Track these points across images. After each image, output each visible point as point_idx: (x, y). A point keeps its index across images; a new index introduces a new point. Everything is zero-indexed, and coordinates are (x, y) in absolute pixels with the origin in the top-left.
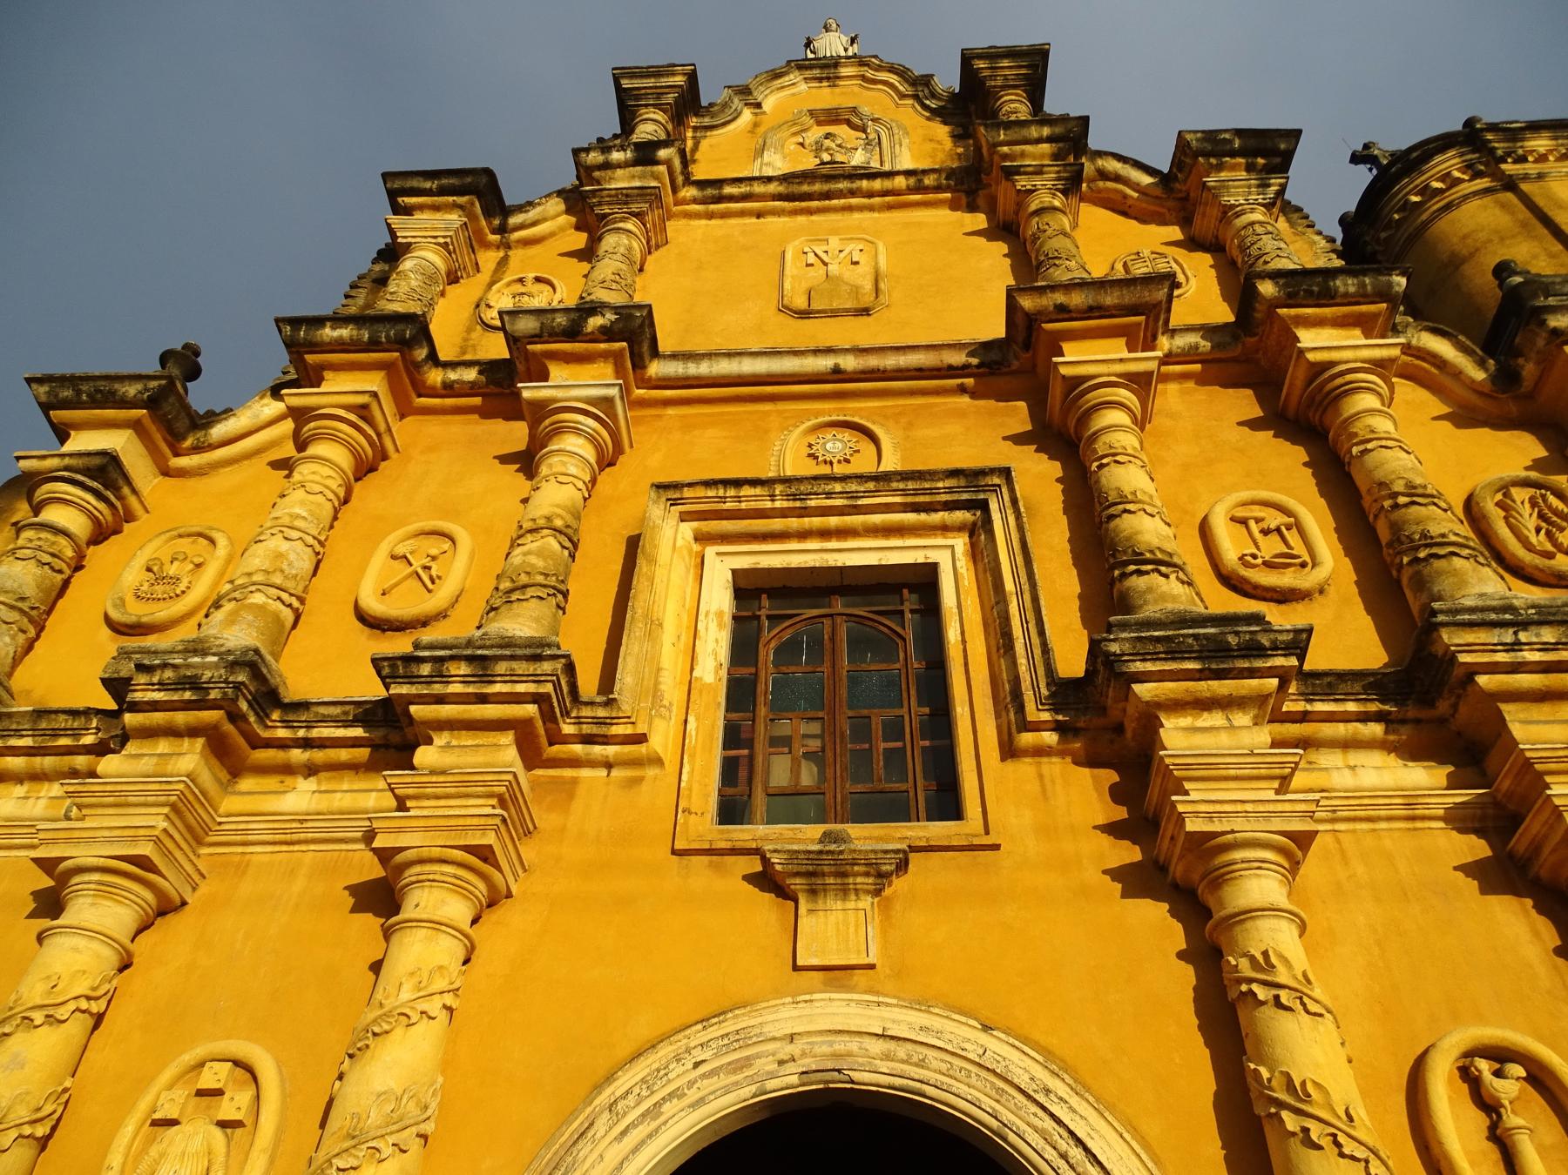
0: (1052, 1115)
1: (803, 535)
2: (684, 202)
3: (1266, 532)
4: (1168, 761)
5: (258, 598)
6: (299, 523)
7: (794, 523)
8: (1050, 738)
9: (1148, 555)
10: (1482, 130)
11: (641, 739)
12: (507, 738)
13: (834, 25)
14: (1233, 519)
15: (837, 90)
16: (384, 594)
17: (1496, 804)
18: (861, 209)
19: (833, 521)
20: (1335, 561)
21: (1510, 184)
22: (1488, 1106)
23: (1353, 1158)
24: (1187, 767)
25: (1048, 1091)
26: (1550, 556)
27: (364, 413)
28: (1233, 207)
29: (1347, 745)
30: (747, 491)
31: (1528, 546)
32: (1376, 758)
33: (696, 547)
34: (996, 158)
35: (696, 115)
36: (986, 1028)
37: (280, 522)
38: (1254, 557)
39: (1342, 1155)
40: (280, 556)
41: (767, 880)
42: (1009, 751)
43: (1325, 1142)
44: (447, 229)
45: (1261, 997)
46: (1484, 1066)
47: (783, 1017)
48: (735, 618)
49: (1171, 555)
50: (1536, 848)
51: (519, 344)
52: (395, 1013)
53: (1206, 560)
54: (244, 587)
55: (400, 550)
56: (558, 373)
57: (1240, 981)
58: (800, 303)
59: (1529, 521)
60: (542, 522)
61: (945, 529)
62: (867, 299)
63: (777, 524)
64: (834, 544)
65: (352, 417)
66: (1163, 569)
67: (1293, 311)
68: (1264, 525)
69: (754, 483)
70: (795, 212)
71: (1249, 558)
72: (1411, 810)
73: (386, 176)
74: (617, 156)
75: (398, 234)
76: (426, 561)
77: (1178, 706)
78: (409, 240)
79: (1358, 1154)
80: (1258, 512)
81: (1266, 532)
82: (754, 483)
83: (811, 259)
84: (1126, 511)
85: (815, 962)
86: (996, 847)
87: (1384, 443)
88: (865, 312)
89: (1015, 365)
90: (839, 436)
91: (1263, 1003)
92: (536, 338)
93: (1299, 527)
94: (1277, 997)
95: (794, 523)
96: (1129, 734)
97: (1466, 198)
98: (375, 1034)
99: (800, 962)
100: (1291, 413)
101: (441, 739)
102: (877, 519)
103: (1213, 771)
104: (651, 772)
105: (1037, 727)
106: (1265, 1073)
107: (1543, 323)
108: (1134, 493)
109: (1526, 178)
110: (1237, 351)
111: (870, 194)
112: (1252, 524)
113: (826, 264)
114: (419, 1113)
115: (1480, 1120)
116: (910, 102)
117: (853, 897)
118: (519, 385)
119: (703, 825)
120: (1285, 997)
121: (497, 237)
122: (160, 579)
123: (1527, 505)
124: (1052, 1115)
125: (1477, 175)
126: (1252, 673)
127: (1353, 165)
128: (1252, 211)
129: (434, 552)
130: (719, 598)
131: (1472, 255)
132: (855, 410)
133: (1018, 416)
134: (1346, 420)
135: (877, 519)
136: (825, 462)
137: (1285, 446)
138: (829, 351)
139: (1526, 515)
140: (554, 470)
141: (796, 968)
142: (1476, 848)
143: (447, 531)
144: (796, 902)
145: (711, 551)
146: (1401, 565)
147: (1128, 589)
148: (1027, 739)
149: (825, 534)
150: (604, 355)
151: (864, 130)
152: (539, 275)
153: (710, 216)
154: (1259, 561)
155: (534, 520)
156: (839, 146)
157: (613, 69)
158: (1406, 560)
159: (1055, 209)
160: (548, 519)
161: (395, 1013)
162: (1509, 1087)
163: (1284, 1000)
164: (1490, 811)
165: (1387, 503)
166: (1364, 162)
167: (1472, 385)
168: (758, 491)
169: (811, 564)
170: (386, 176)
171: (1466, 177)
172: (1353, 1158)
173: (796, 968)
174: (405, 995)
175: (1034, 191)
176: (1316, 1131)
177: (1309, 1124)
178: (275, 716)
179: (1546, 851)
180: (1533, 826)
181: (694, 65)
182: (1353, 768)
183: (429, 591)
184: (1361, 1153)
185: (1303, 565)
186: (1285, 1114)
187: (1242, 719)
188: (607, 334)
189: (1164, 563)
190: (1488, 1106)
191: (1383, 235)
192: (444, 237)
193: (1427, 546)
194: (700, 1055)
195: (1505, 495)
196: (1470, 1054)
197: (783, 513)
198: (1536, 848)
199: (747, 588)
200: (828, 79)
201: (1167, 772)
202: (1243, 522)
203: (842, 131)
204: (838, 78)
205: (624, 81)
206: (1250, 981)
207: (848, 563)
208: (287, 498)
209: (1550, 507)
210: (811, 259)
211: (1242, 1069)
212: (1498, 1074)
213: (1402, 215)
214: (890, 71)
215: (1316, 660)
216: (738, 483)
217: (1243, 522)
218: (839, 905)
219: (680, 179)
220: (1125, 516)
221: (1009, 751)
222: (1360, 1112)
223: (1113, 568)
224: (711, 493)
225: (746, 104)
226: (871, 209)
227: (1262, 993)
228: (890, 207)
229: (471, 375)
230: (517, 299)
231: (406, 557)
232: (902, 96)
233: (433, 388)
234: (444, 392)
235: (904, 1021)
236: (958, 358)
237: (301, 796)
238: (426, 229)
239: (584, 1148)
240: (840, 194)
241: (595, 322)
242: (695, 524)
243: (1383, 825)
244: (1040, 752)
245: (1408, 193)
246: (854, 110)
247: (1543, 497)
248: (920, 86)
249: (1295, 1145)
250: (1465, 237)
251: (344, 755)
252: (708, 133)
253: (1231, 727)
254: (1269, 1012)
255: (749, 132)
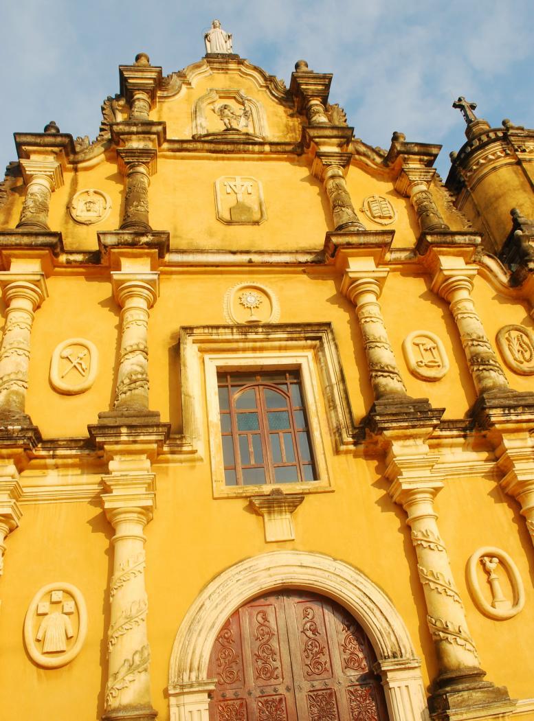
0: (359, 589)
1: (244, 350)
2: (163, 151)
3: (426, 350)
4: (396, 462)
5: (15, 388)
6: (22, 346)
7: (241, 345)
8: (352, 447)
9: (386, 369)
10: (510, 135)
11: (194, 452)
12: (144, 457)
13: (218, 24)
14: (414, 344)
15: (227, 76)
16: (63, 377)
17: (498, 467)
18: (249, 159)
19: (258, 344)
20: (451, 366)
21: (519, 162)
22: (488, 572)
23: (450, 596)
24: (402, 464)
25: (357, 581)
26: (522, 363)
27: (37, 283)
28: (414, 181)
29: (451, 446)
30: (221, 330)
31: (515, 359)
32: (459, 450)
33: (200, 354)
34: (312, 143)
35: (160, 90)
36: (335, 560)
37: (13, 346)
38: (421, 362)
39: (447, 595)
40: (18, 364)
41: (251, 508)
42: (337, 452)
43: (443, 592)
44: (52, 168)
45: (425, 546)
46: (486, 559)
47: (264, 561)
48: (219, 387)
49: (394, 368)
50: (508, 484)
51: (107, 249)
52: (130, 572)
53: (404, 362)
54: (7, 381)
55: (65, 354)
56: (33, 157)
57: (417, 540)
58: (227, 216)
59: (516, 347)
60: (135, 347)
61: (304, 348)
62: (256, 216)
63: (234, 345)
64: (258, 354)
65: (33, 286)
66: (391, 375)
67: (439, 249)
68: (425, 347)
69: (224, 327)
70: (217, 159)
71: (420, 363)
72: (471, 471)
73: (16, 135)
75: (26, 169)
76: (78, 361)
77: (398, 438)
78: (32, 173)
79: (452, 595)
80: (425, 341)
81: (426, 350)
82: (224, 327)
83: (229, 190)
84: (376, 346)
85: (273, 540)
86: (333, 491)
87: (470, 315)
88: (256, 223)
89: (327, 262)
90: (253, 294)
91: (425, 548)
92: (114, 246)
93: (436, 348)
94: (429, 546)
95: (241, 345)
96: (380, 445)
97: (501, 166)
98: (124, 581)
99: (268, 540)
100: (435, 290)
101: (117, 458)
102: (277, 344)
103: (411, 466)
104: (198, 464)
105: (347, 444)
106: (425, 571)
107: (527, 265)
108: (380, 338)
109: (525, 160)
110: (415, 260)
111: (253, 152)
112: (421, 346)
113: (236, 193)
115: (485, 576)
116: (264, 89)
117: (284, 514)
118: (112, 272)
120: (432, 546)
121: (71, 166)
123: (516, 339)
124: (359, 589)
125: (507, 155)
126: (423, 426)
127: (454, 108)
128: (422, 184)
129: (81, 355)
131: (503, 195)
132: (260, 281)
133: (328, 288)
134: (456, 302)
135: (277, 344)
136: (248, 307)
137: (434, 307)
138: (248, 252)
139: (515, 344)
140: (135, 318)
142: (492, 484)
143: (89, 347)
144: (263, 516)
145: (207, 357)
146: (473, 370)
147: (378, 383)
148: (343, 448)
149: (254, 349)
150: (148, 255)
151: (243, 104)
152: (96, 190)
153: (175, 158)
154: (423, 364)
155: (131, 346)
156: (232, 113)
157: (120, 66)
158: (475, 369)
159: (340, 176)
160: (138, 345)
161: (130, 572)
162: (493, 565)
163: (432, 547)
164: (495, 470)
165: (470, 343)
166: (459, 107)
167: (501, 282)
168: (227, 331)
169: (250, 364)
170: (16, 135)
171: (503, 155)
172: (450, 596)
173: (267, 542)
174: (132, 565)
175: (330, 165)
176: (440, 589)
177: (438, 586)
178: (40, 445)
179: (511, 486)
180: (507, 478)
181: (161, 67)
182: (453, 453)
183: (83, 376)
184: (452, 594)
185: (439, 366)
186: (431, 583)
187: (419, 441)
188: (149, 245)
189: (390, 372)
190: (488, 572)
191: (469, 174)
192: (50, 172)
193: (483, 365)
194: (238, 577)
195: (509, 335)
196: (483, 556)
197: (237, 341)
198: (508, 484)
200: (223, 69)
201: (395, 465)
202: (418, 345)
203: (232, 103)
204: (228, 69)
205: (125, 73)
206: (422, 540)
207: (265, 363)
208: (12, 332)
209: (523, 341)
210: (229, 190)
211: (417, 568)
212: (491, 562)
213: (477, 167)
214: (253, 70)
215: (446, 416)
216: (217, 327)
217: (418, 345)
218: (279, 517)
219: (162, 140)
220: (376, 348)
221: (337, 452)
222: (452, 581)
223: (372, 371)
224: (206, 331)
225: (183, 83)
226: (253, 159)
227: (425, 544)
228: (261, 159)
229: (79, 258)
230: (88, 205)
231: (67, 358)
232: (261, 86)
233: (62, 263)
234: (67, 265)
235: (307, 559)
236: (303, 258)
237: (53, 477)
238: (40, 167)
239: (202, 613)
240: (239, 152)
242: (199, 345)
243: (462, 476)
244: (347, 452)
245: (480, 158)
246: (238, 92)
247: (521, 336)
248: (270, 80)
249: (434, 594)
250: (500, 185)
251: (70, 461)
252: (166, 100)
253: (416, 445)
254: (427, 551)
255: (186, 100)
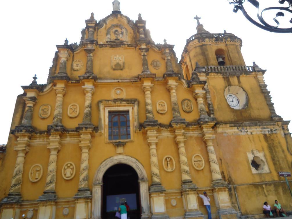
32: (232, 105)
54: (57, 116)
62: (122, 67)
74: (89, 42)
88: (122, 70)
114: (159, 136)
119: (108, 141)
122: (44, 112)
130: (107, 114)
141: (233, 101)
199: (110, 112)
202: (160, 105)
239: (101, 169)
241: (90, 77)
